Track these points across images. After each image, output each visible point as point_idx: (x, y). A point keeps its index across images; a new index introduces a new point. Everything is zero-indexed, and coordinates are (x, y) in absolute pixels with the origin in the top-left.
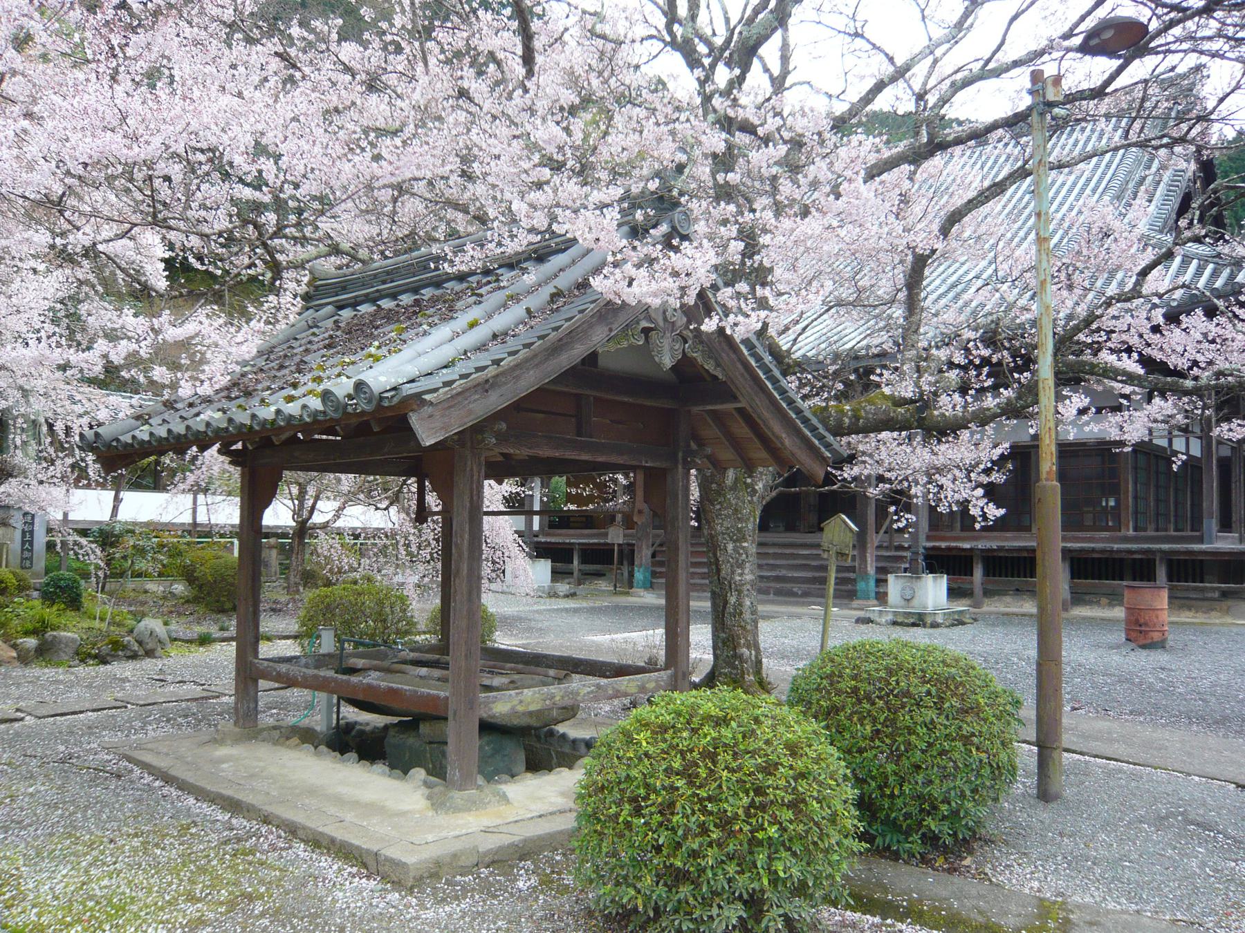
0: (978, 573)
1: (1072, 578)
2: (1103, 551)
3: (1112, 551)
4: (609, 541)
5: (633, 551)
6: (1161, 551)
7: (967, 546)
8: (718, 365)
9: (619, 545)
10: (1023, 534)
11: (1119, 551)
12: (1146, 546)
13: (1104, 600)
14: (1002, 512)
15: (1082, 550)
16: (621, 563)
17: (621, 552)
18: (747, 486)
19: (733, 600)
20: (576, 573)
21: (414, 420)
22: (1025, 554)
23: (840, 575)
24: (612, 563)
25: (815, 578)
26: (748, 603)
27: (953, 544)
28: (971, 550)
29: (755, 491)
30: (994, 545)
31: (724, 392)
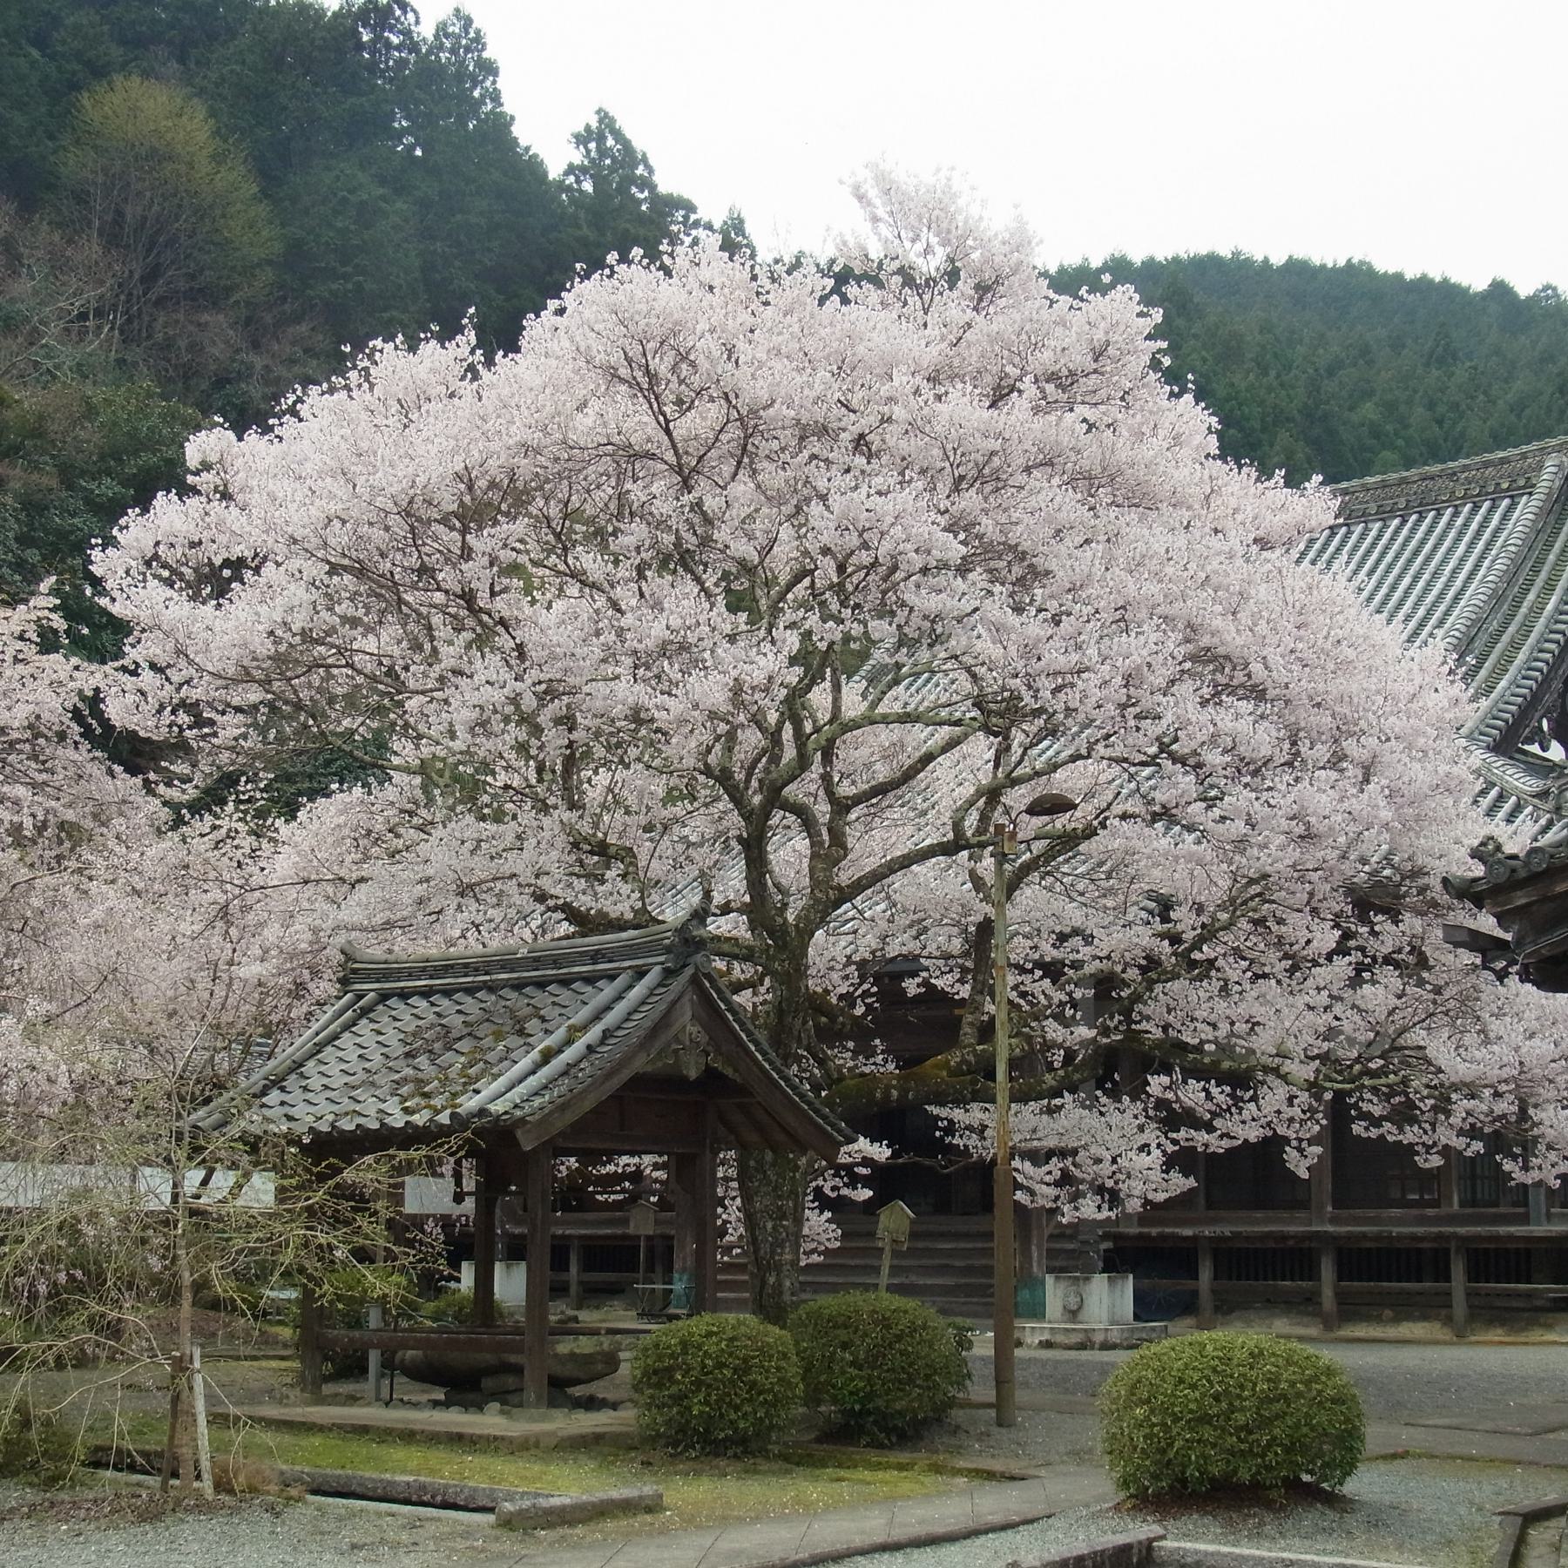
0: (1205, 1274)
1: (1340, 1279)
2: (1378, 1237)
3: (1390, 1237)
4: (631, 1231)
5: (670, 1249)
6: (1455, 1236)
7: (1188, 1232)
8: (736, 1070)
9: (649, 1238)
10: (1302, 1214)
11: (1400, 1237)
12: (1435, 1230)
13: (1388, 1313)
14: (1191, 1182)
15: (1350, 1237)
16: (651, 1268)
17: (651, 1250)
18: (789, 1161)
19: (772, 1280)
20: (573, 1289)
21: (519, 1133)
22: (1272, 1244)
23: (896, 1262)
24: (635, 1269)
25: (958, 1286)
26: (788, 1283)
27: (1168, 1230)
28: (1195, 1238)
29: (797, 1168)
30: (1227, 1230)
31: (742, 1090)
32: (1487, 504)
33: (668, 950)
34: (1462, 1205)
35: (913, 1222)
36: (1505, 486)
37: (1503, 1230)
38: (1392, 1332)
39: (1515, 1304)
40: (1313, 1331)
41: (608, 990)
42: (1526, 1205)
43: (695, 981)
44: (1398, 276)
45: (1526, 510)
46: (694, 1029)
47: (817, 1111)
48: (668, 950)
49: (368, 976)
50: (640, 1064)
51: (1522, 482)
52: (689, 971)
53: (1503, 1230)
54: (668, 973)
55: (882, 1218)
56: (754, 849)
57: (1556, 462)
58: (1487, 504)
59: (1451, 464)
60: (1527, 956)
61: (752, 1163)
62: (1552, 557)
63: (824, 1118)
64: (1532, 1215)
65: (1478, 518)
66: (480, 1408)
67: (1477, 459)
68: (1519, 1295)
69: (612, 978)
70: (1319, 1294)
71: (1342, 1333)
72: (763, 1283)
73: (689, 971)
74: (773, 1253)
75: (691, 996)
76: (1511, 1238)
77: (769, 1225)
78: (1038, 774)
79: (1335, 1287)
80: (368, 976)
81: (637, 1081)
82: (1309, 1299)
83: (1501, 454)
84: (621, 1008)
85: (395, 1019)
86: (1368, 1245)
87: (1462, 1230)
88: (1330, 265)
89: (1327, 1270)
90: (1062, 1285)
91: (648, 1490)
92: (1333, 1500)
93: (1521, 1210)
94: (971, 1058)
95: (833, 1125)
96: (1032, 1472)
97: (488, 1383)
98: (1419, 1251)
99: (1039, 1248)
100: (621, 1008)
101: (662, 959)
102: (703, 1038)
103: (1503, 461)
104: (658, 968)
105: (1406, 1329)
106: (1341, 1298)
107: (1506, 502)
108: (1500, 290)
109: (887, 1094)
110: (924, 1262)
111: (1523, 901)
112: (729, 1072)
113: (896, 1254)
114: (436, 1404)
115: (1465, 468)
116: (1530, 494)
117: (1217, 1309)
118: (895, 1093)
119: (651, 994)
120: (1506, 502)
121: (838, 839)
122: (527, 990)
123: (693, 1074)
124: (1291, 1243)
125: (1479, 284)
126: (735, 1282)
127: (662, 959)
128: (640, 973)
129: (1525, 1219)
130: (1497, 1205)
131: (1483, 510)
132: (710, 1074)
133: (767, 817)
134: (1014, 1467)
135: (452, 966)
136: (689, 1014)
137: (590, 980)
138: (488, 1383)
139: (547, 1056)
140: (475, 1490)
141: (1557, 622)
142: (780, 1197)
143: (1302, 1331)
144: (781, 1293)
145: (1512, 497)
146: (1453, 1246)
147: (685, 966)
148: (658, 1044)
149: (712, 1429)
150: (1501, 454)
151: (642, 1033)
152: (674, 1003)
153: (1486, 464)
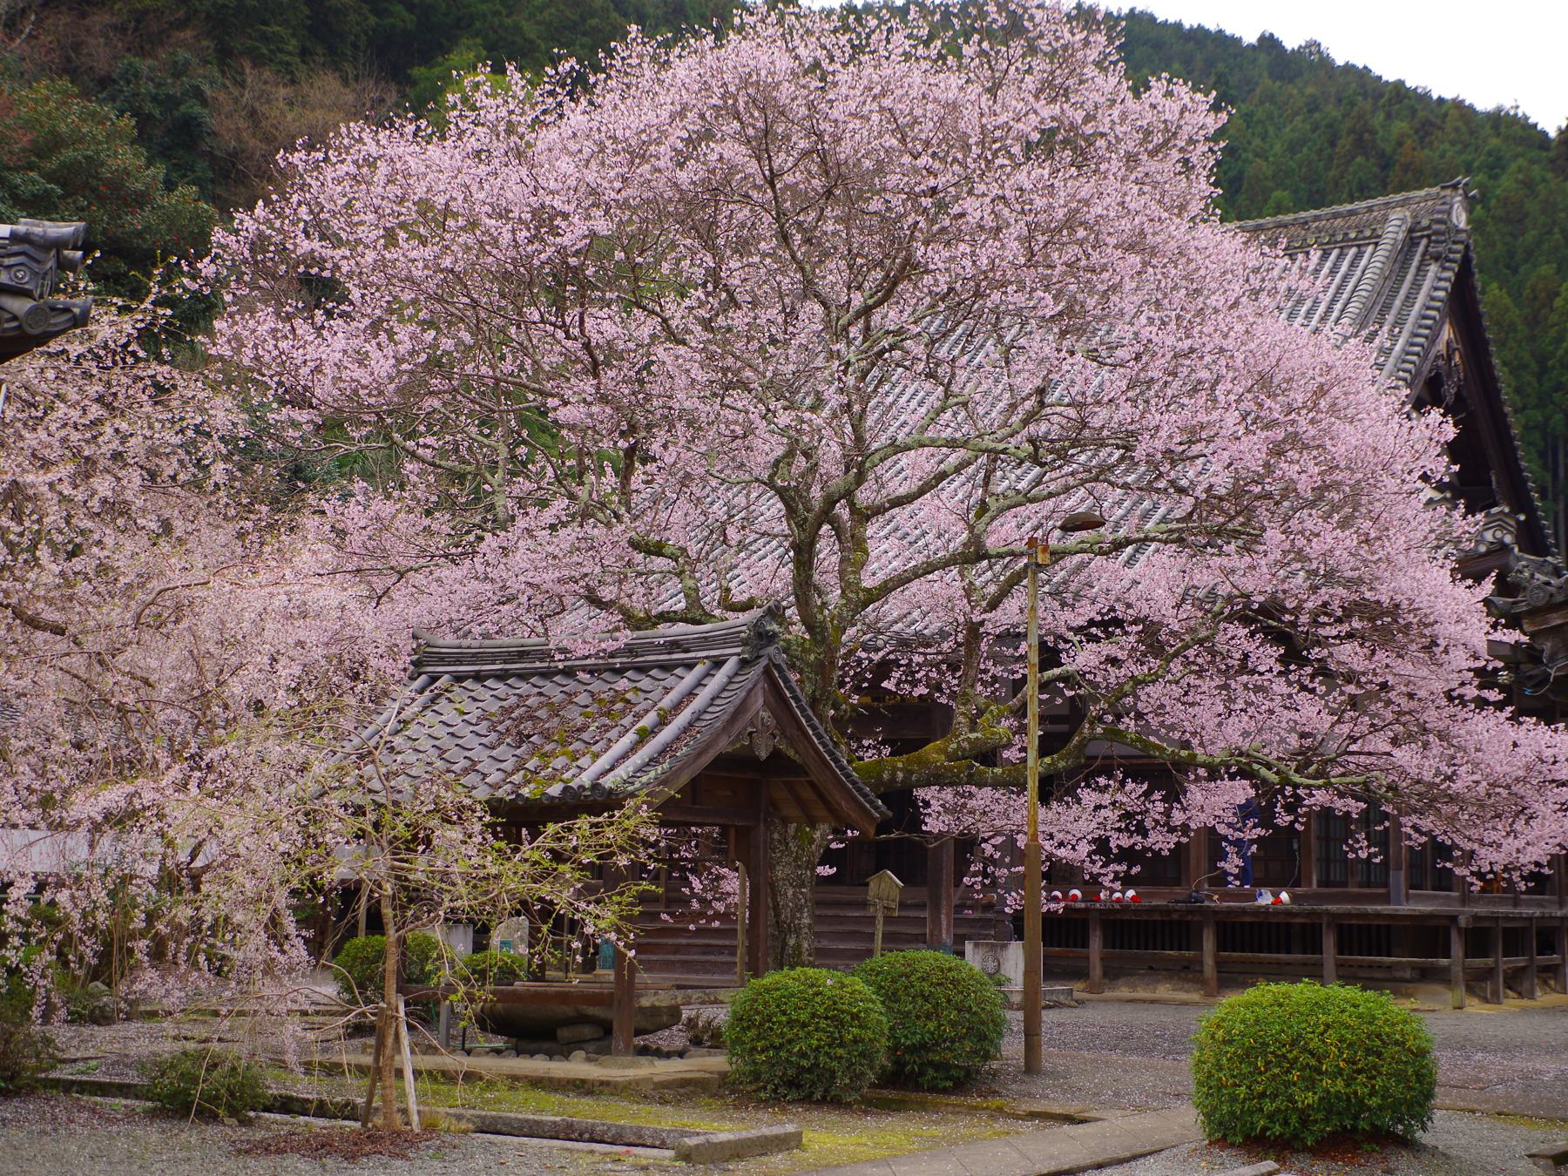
0: (1096, 945)
6: (1327, 912)
19: (792, 942)
29: (812, 841)
32: (1335, 253)
33: (744, 643)
34: (1319, 885)
35: (902, 890)
36: (1353, 235)
37: (1370, 908)
38: (1141, 994)
39: (1376, 975)
40: (1195, 997)
41: (690, 677)
42: (1386, 885)
43: (767, 672)
44: (1178, 26)
45: (1375, 261)
46: (765, 714)
47: (859, 790)
48: (744, 643)
49: (442, 659)
50: (723, 746)
51: (1368, 233)
52: (764, 662)
53: (1370, 908)
54: (744, 664)
55: (872, 885)
56: (804, 554)
57: (1400, 215)
58: (1335, 253)
59: (1303, 214)
60: (1559, 670)
61: (776, 836)
62: (1398, 303)
63: (865, 796)
64: (1392, 894)
65: (1329, 264)
66: (566, 1056)
67: (1327, 210)
68: (1380, 966)
69: (690, 666)
70: (1201, 962)
71: (1108, 994)
72: (785, 944)
73: (764, 662)
74: (793, 917)
75: (763, 685)
76: (1378, 915)
77: (790, 893)
78: (1051, 495)
79: (1216, 956)
80: (442, 659)
81: (721, 761)
82: (1187, 968)
83: (1349, 207)
84: (704, 695)
85: (475, 700)
86: (1247, 919)
87: (1332, 908)
88: (1187, 26)
89: (1329, 942)
90: (981, 951)
91: (790, 1128)
92: (1407, 1143)
93: (1382, 891)
94: (965, 745)
95: (871, 802)
96: (1093, 1114)
97: (564, 1033)
98: (1288, 925)
99: (948, 915)
100: (704, 695)
101: (738, 650)
102: (771, 722)
103: (1352, 213)
104: (735, 658)
105: (1164, 991)
106: (1219, 964)
107: (1353, 250)
108: (1269, 43)
109: (894, 775)
110: (840, 928)
111: (1559, 622)
112: (791, 753)
113: (888, 920)
114: (498, 1052)
115: (1317, 218)
116: (1376, 244)
117: (1105, 974)
118: (900, 775)
119: (730, 682)
120: (1353, 250)
121: (859, 544)
122: (653, 672)
123: (763, 755)
124: (1175, 916)
125: (1250, 37)
126: (657, 944)
127: (738, 650)
128: (718, 663)
129: (1386, 899)
130: (1345, 885)
131: (1333, 257)
132: (776, 754)
133: (820, 527)
134: (1072, 1108)
135: (528, 653)
136: (761, 701)
137: (667, 668)
138: (564, 1033)
139: (644, 736)
140: (623, 1128)
141: (1404, 361)
142: (799, 867)
143: (1183, 996)
144: (800, 954)
145: (1359, 246)
146: (1325, 921)
147: (759, 657)
148: (735, 731)
149: (800, 1074)
150: (1349, 207)
151: (725, 717)
152: (750, 691)
153: (1336, 216)
